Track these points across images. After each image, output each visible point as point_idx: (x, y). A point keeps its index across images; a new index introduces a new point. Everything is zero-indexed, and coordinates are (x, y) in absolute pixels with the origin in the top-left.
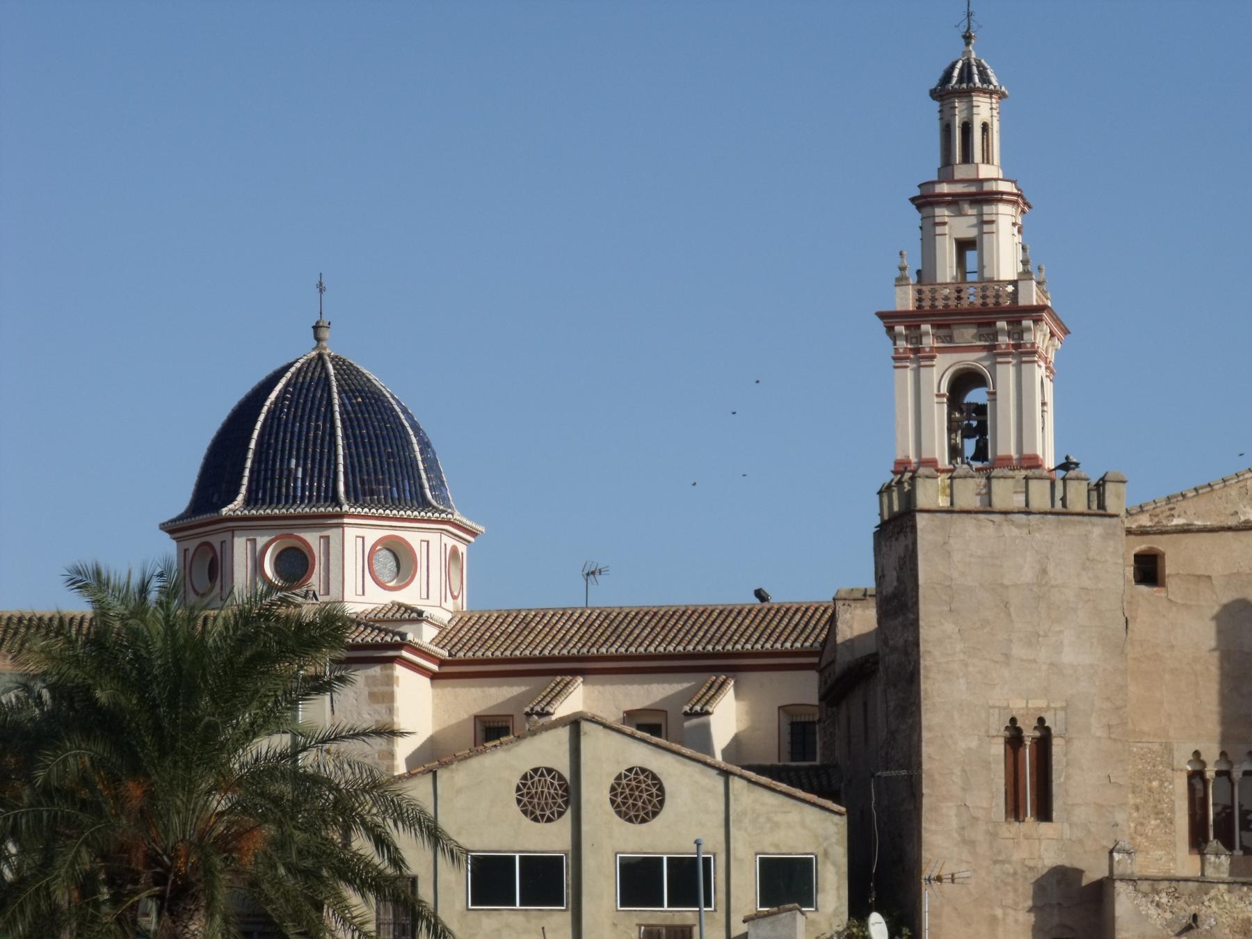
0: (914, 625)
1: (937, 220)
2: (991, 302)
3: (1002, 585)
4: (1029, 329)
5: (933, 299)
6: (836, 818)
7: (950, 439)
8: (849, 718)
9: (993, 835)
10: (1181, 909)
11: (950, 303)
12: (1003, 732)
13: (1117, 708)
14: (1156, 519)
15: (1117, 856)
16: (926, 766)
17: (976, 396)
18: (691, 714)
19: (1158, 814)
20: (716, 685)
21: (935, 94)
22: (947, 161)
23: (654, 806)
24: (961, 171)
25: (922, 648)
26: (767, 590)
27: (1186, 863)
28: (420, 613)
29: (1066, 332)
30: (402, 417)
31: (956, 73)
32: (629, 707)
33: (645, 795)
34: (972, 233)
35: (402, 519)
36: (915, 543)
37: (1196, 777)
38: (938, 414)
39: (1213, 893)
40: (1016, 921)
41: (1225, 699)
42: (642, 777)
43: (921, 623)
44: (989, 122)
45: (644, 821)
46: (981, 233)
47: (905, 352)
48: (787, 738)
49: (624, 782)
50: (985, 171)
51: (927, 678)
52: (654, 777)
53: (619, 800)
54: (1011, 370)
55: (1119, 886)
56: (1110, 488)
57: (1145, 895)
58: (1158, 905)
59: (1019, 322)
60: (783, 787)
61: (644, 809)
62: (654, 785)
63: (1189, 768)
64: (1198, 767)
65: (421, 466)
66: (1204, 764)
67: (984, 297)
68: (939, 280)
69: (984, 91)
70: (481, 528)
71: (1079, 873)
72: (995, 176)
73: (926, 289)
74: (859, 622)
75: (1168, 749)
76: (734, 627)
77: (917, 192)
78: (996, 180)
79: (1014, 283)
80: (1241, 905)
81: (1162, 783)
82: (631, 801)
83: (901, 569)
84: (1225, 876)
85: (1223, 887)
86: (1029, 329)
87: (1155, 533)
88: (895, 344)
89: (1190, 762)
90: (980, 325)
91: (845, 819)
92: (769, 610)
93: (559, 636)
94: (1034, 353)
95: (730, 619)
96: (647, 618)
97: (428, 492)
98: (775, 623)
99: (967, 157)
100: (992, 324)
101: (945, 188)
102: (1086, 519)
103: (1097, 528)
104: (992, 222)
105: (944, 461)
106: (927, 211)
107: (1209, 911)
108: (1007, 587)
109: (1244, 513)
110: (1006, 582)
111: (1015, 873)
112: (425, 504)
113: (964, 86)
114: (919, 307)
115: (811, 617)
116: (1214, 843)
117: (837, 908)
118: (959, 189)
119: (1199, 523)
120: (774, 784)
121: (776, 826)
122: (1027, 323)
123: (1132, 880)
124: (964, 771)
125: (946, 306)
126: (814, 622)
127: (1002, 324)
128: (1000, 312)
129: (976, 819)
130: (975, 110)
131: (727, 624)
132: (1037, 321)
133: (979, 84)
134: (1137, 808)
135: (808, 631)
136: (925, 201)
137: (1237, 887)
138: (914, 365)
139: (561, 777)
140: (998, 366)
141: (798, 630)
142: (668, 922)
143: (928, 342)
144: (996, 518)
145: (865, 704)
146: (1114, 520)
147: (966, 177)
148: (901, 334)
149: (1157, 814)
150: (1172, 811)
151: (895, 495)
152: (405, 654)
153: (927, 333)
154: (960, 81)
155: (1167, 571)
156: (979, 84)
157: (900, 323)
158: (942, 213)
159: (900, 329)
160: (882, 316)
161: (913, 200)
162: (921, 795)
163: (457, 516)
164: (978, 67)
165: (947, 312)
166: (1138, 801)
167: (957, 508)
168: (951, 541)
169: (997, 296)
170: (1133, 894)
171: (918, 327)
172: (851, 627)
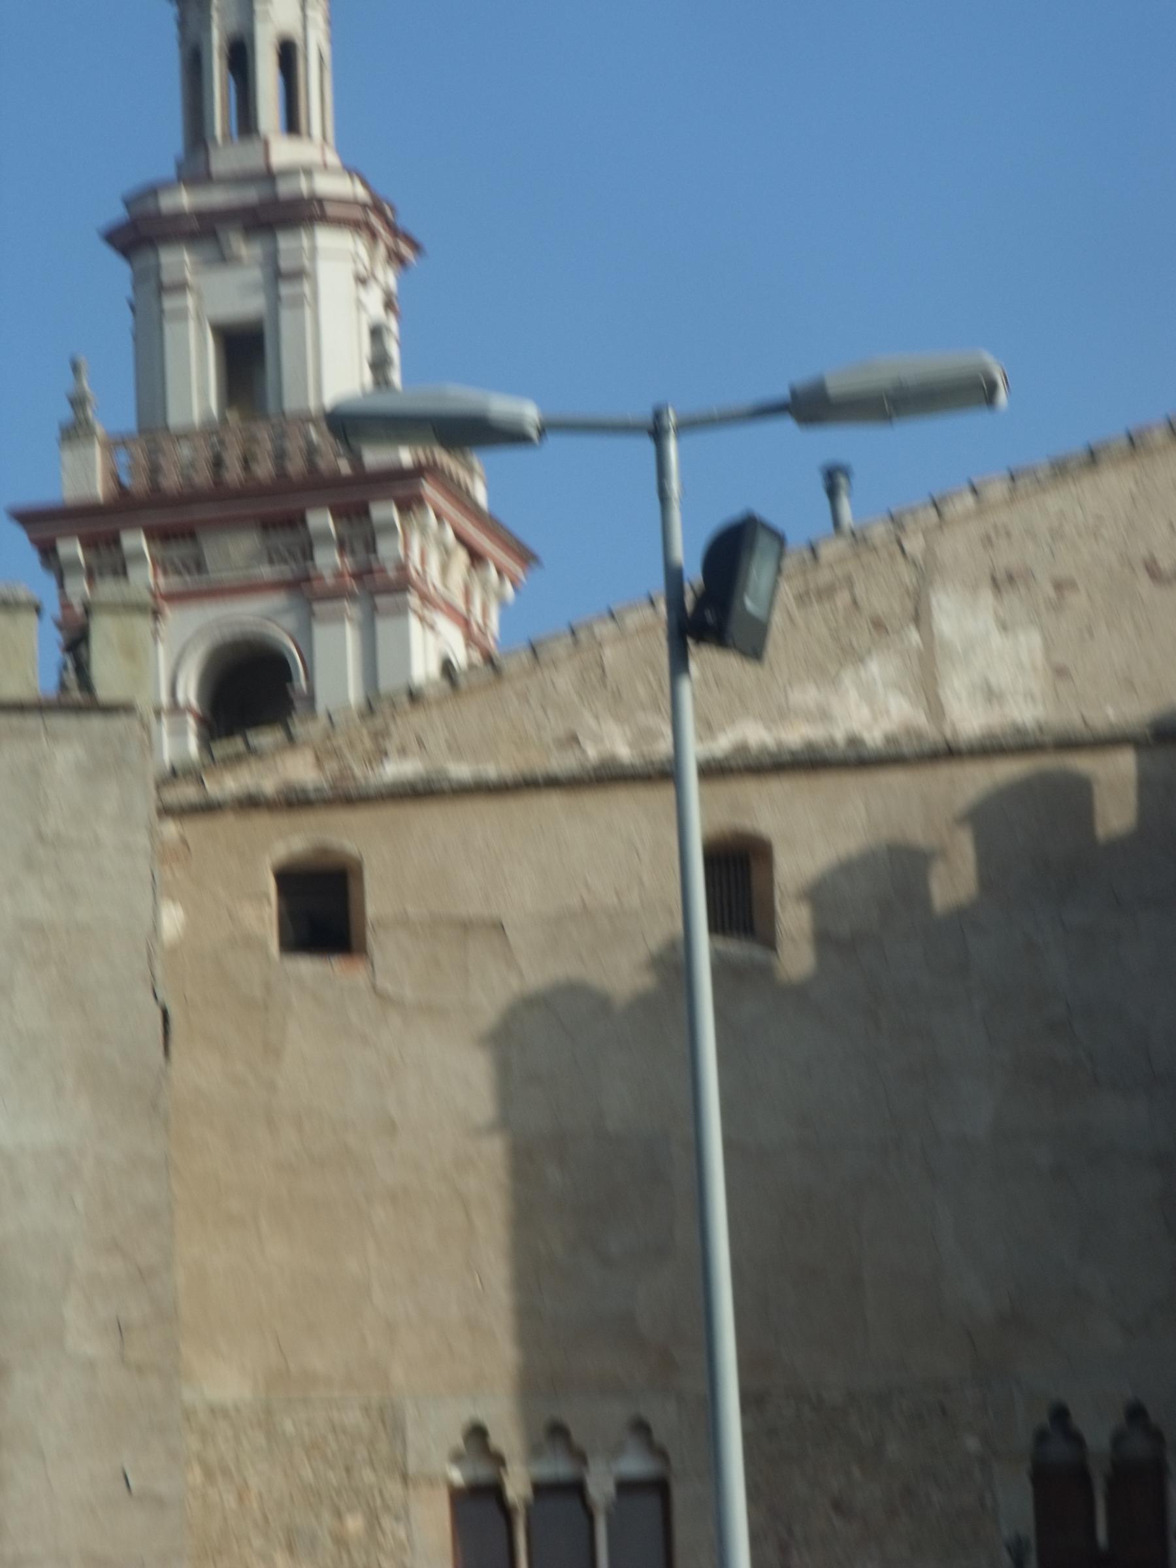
22: (197, 132)
24: (227, 157)
29: (526, 556)
41: (532, 1276)
44: (296, 33)
46: (275, 301)
50: (284, 152)
54: (351, 636)
63: (457, 1476)
64: (483, 1472)
66: (499, 1460)
75: (390, 1420)
81: (373, 1521)
88: (61, 585)
90: (268, 525)
99: (246, 119)
100: (295, 521)
101: (184, 200)
102: (32, 722)
118: (216, 198)
119: (461, 771)
122: (385, 511)
127: (321, 520)
128: (319, 486)
132: (410, 504)
136: (139, 235)
146: (118, 724)
158: (178, 261)
159: (72, 549)
160: (28, 519)
165: (189, 498)
171: (115, 541)
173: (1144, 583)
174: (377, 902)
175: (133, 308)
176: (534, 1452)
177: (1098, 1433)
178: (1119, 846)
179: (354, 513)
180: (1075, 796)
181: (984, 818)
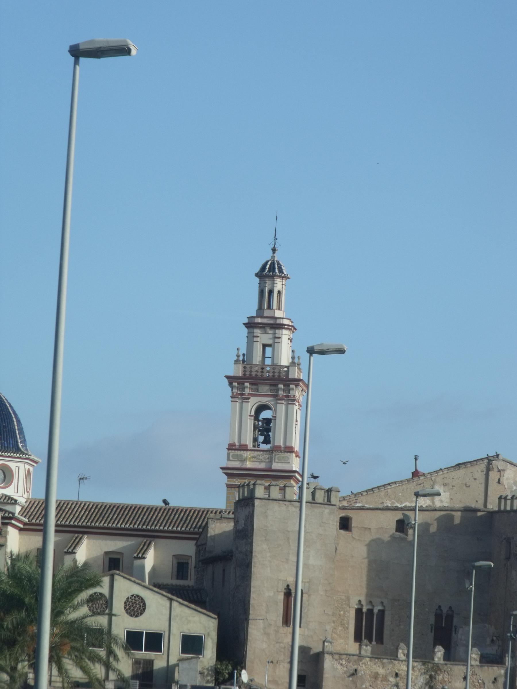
0: (251, 544)
1: (255, 335)
2: (276, 375)
3: (287, 531)
4: (293, 389)
5: (251, 371)
6: (214, 620)
7: (254, 434)
8: (213, 573)
9: (277, 632)
10: (350, 666)
11: (258, 374)
12: (283, 590)
13: (330, 584)
14: (350, 503)
15: (326, 644)
16: (252, 602)
17: (266, 414)
18: (137, 558)
19: (342, 625)
20: (147, 544)
21: (257, 275)
22: (260, 307)
23: (141, 611)
24: (267, 313)
25: (253, 554)
26: (169, 500)
27: (353, 647)
28: (16, 501)
30: (10, 409)
31: (268, 267)
32: (106, 550)
33: (138, 606)
34: (270, 342)
35: (9, 457)
36: (253, 511)
37: (359, 612)
38: (249, 424)
39: (364, 661)
40: (284, 667)
42: (137, 599)
43: (254, 544)
44: (281, 290)
45: (137, 616)
47: (236, 395)
48: (175, 569)
49: (130, 600)
50: (278, 314)
51: (254, 566)
52: (142, 599)
53: (127, 607)
54: (283, 407)
55: (326, 656)
56: (333, 494)
57: (336, 660)
58: (341, 664)
59: (289, 386)
60: (193, 606)
61: (137, 611)
62: (142, 602)
63: (356, 607)
64: (360, 607)
65: (17, 432)
66: (362, 605)
67: (274, 372)
68: (254, 363)
69: (280, 276)
70: (40, 461)
71: (310, 649)
72: (282, 317)
73: (248, 366)
74: (218, 528)
75: (348, 599)
76: (154, 517)
77: (246, 321)
78: (283, 318)
79: (288, 367)
80: (374, 667)
81: (344, 613)
82: (132, 608)
83: (246, 520)
84: (369, 654)
85: (368, 659)
86: (293, 389)
87: (349, 509)
88: (232, 390)
89: (357, 604)
90: (271, 385)
91: (217, 621)
92: (169, 509)
93: (77, 515)
94: (294, 400)
95: (152, 513)
96: (115, 509)
97: (20, 444)
98: (172, 517)
99: (269, 307)
100: (276, 385)
101: (259, 320)
102: (322, 506)
103: (327, 510)
104: (279, 338)
105: (250, 446)
106: (251, 330)
107: (362, 668)
108: (289, 531)
109: (386, 503)
110: (289, 529)
111: (285, 648)
112: (18, 450)
113: (271, 273)
114: (244, 375)
115: (188, 515)
116: (365, 641)
117: (211, 657)
118: (265, 321)
120: (189, 605)
121: (189, 622)
122: (292, 386)
123: (331, 654)
124: (267, 604)
125: (256, 375)
126: (189, 518)
127: (281, 386)
128: (280, 379)
129: (271, 625)
130: (275, 285)
131: (151, 515)
132: (297, 386)
133: (278, 274)
134: (334, 622)
135: (187, 522)
136: (250, 325)
137: (373, 659)
138: (240, 401)
139: (105, 597)
140: (278, 405)
141: (183, 521)
142: (144, 658)
143: (247, 391)
144: (287, 503)
145: (224, 570)
146: (334, 507)
147: (269, 315)
148: (235, 386)
149: (342, 625)
150: (348, 624)
151: (246, 490)
152: (13, 522)
153: (247, 387)
154: (269, 271)
155: (353, 525)
156: (278, 274)
157: (235, 382)
158: (257, 331)
159: (235, 384)
160: (228, 377)
161: (244, 324)
162: (249, 614)
163: (33, 457)
164: (278, 265)
165: (256, 378)
166: (335, 619)
167: (271, 498)
168: (268, 511)
169: (280, 373)
170: (332, 659)
172: (214, 531)
173: (464, 487)
174: (354, 524)
175: (247, 337)
176: (367, 605)
177: (445, 610)
178: (456, 525)
179: (287, 386)
180: (451, 518)
181: (438, 519)
